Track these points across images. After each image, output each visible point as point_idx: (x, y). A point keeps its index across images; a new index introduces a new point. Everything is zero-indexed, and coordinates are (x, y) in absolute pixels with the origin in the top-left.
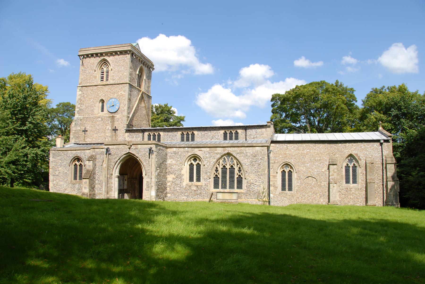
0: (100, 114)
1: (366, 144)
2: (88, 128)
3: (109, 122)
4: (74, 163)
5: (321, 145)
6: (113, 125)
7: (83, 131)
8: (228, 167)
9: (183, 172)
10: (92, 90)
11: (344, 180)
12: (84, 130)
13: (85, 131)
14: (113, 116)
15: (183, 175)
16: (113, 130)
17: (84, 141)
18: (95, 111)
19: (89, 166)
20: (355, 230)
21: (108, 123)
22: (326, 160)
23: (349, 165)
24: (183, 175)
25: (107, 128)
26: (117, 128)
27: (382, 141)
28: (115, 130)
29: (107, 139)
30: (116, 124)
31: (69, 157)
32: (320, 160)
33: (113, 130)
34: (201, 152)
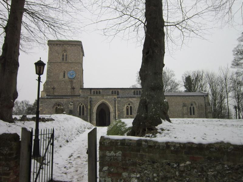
0: (63, 79)
1: (54, 160)
2: (56, 86)
3: (70, 83)
4: (56, 107)
5: (179, 98)
6: (72, 86)
7: (52, 88)
8: (82, 106)
9: (124, 110)
10: (58, 65)
11: (190, 114)
12: (53, 87)
13: (54, 88)
14: (71, 81)
15: (124, 112)
16: (72, 88)
17: (53, 94)
18: (60, 77)
19: (71, 108)
20: (143, 64)
21: (69, 84)
22: (181, 105)
23: (191, 107)
24: (124, 112)
25: (68, 87)
26: (74, 87)
27: (205, 96)
28: (73, 88)
29: (68, 94)
30: (74, 85)
31: (53, 103)
32: (179, 104)
33: (72, 88)
34: (132, 100)
